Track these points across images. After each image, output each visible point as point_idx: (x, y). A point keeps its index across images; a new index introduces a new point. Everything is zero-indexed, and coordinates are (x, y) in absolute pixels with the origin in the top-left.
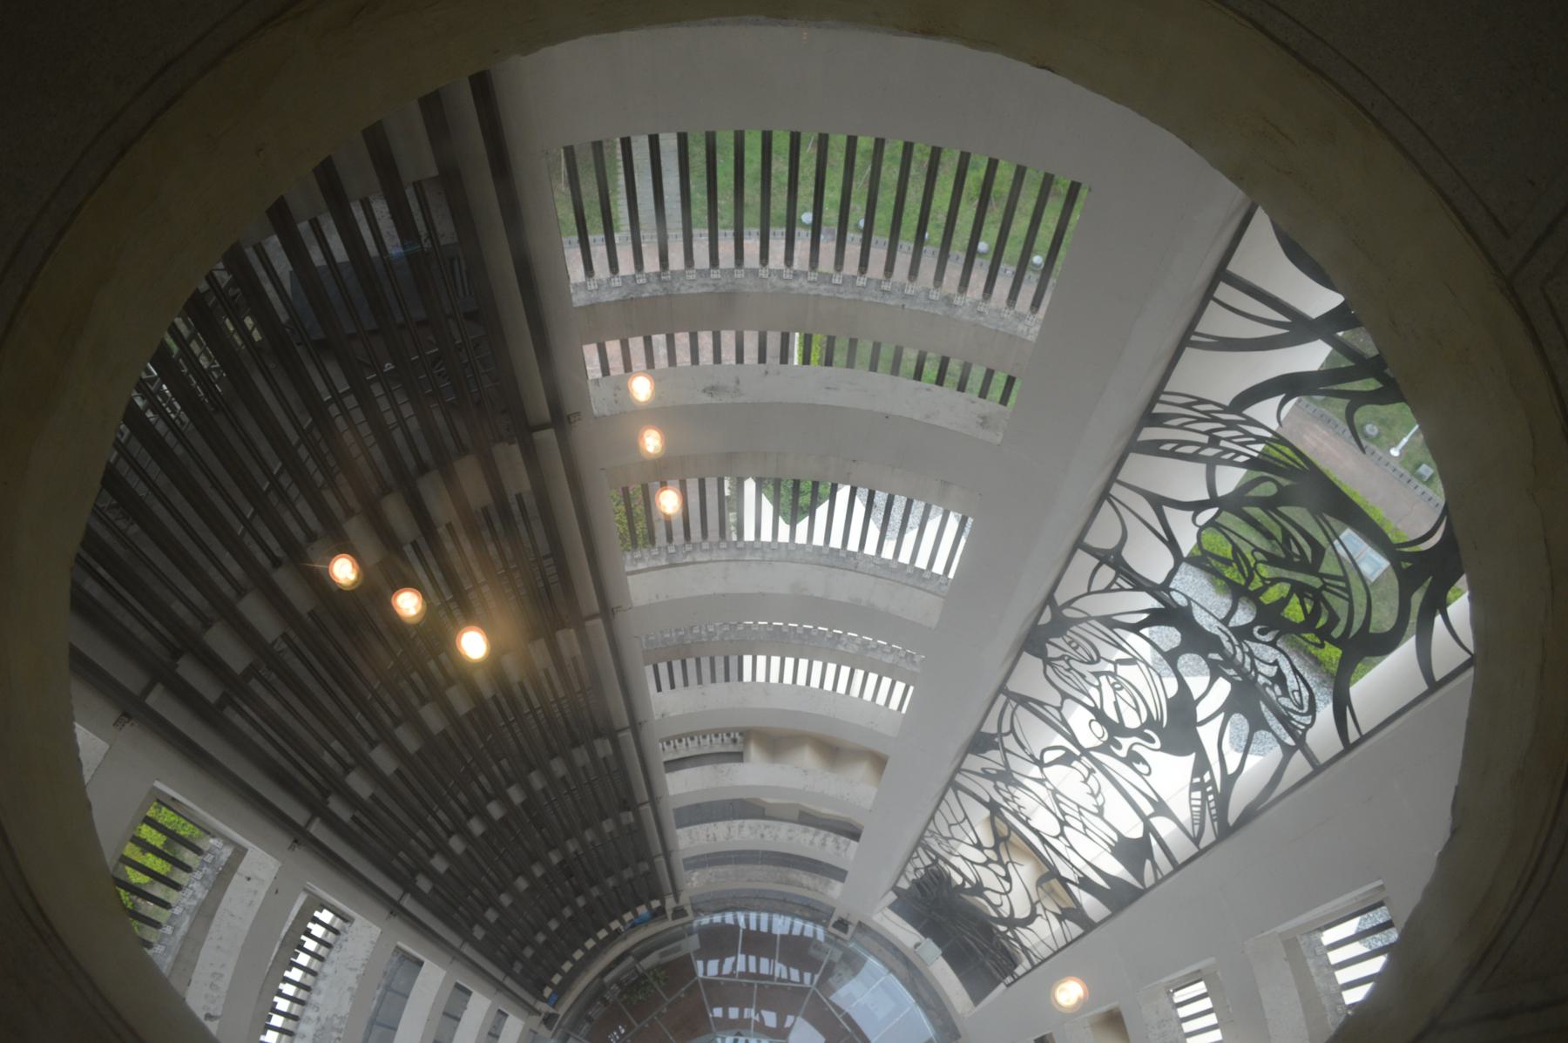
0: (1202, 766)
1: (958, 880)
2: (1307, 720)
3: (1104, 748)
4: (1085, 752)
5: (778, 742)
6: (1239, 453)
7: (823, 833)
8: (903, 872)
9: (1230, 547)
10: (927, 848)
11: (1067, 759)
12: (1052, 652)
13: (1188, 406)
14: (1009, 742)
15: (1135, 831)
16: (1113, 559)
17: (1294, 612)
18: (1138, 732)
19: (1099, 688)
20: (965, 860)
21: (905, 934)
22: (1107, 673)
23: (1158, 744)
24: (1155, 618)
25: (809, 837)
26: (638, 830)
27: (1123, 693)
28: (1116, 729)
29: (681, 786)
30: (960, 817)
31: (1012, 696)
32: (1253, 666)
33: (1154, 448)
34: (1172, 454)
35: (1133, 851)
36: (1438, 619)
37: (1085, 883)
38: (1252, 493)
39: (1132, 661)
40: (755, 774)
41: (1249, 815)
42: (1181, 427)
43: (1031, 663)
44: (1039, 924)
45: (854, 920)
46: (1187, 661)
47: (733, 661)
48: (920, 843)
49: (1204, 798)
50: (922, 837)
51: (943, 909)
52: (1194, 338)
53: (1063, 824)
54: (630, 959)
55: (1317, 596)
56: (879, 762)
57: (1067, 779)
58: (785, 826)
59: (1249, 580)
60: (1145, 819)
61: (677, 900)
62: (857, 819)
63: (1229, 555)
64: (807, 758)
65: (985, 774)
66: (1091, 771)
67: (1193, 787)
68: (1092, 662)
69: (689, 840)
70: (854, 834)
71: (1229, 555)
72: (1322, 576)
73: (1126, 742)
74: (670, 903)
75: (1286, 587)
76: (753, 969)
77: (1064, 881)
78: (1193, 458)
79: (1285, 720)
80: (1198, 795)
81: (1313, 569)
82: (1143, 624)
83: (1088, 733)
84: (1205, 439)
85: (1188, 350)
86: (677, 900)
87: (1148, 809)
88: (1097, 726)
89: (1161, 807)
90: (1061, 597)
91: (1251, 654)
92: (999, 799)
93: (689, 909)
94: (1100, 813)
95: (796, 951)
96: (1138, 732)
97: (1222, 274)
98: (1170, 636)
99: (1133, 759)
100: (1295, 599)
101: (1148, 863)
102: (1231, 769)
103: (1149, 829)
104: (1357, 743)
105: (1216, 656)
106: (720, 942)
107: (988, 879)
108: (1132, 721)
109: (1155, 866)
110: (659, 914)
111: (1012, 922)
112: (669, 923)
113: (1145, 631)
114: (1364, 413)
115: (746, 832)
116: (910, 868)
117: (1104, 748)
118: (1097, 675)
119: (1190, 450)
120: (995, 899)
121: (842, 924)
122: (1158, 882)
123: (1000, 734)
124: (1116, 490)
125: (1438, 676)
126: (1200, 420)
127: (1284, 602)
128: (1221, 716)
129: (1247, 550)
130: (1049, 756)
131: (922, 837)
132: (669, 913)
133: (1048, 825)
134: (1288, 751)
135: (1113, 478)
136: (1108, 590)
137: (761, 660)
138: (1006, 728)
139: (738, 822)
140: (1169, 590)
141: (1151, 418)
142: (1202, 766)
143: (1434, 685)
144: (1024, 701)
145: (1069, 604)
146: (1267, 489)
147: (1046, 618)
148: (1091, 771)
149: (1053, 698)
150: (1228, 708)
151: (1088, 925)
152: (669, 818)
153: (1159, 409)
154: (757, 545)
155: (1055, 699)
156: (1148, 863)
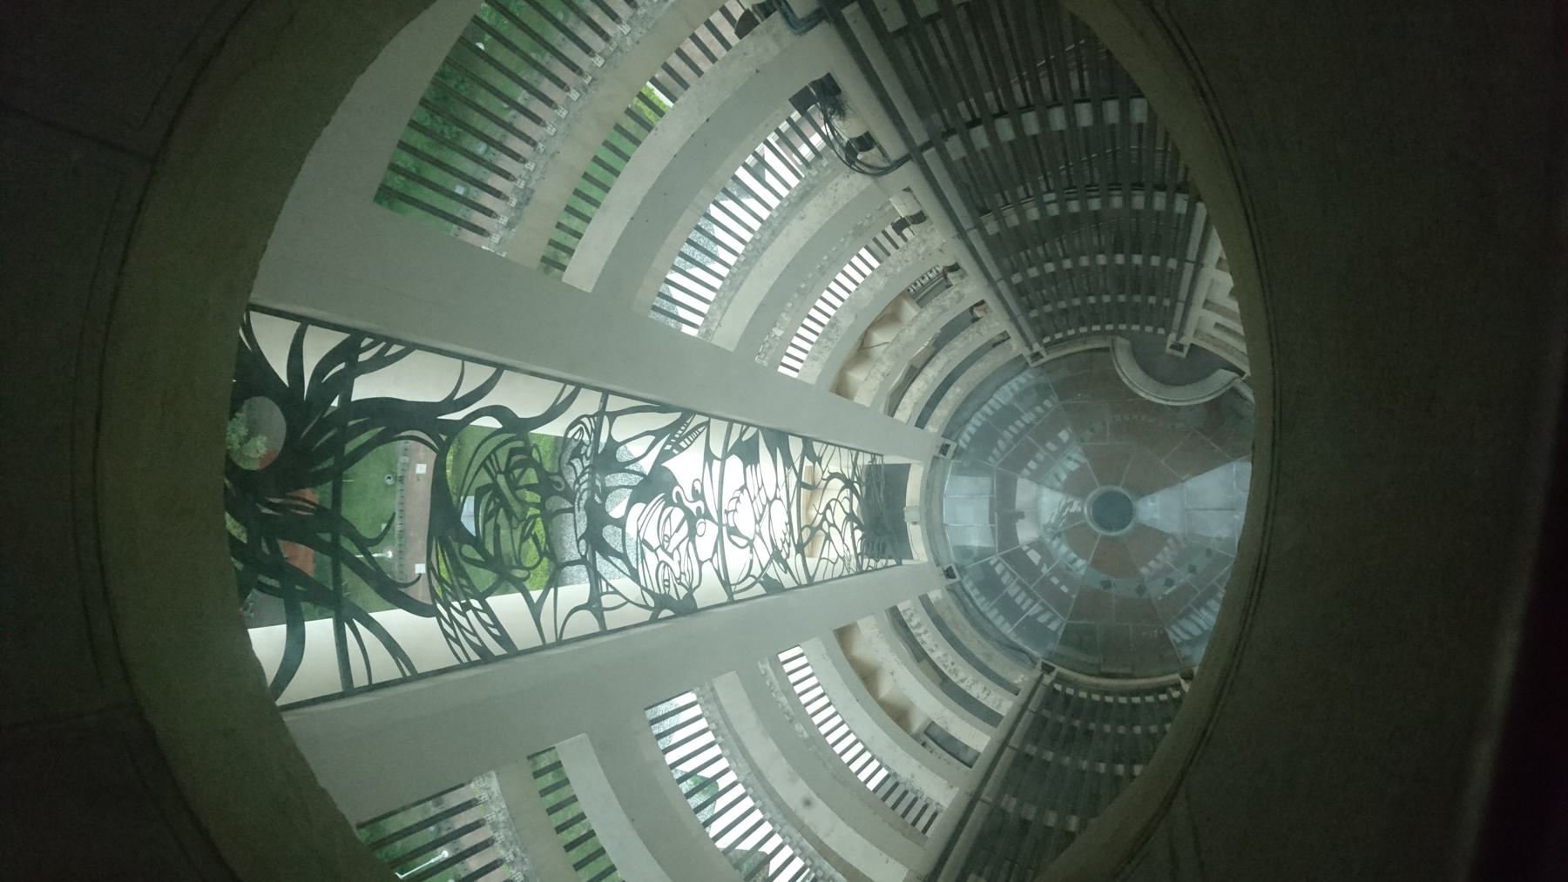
0: (664, 455)
1: (858, 534)
2: (585, 420)
3: (708, 516)
4: (720, 525)
5: (899, 715)
6: (462, 586)
7: (914, 631)
8: (886, 567)
9: (525, 545)
10: (859, 566)
11: (734, 531)
12: (683, 592)
13: (457, 641)
14: (756, 571)
15: (734, 462)
16: (594, 605)
17: (531, 476)
18: (680, 505)
19: (677, 548)
20: (843, 544)
21: (915, 533)
22: (665, 551)
23: (677, 489)
24: (607, 551)
25: (924, 637)
26: (1006, 784)
27: (667, 532)
28: (691, 519)
29: (978, 739)
30: (823, 562)
31: (730, 594)
32: (583, 474)
33: (503, 639)
34: (497, 624)
35: (749, 455)
36: (457, 396)
37: (788, 462)
38: (479, 557)
39: (644, 542)
40: (928, 705)
41: (663, 408)
42: (475, 634)
43: (701, 598)
44: (834, 468)
45: (939, 570)
46: (616, 512)
47: (881, 793)
48: (860, 572)
49: (681, 439)
50: (856, 574)
51: (882, 528)
52: (408, 674)
53: (770, 502)
54: (1103, 670)
55: (508, 472)
56: (844, 635)
57: (744, 520)
58: (934, 656)
59: (534, 517)
60: (723, 461)
61: (1041, 677)
62: (886, 619)
63: (530, 541)
64: (886, 689)
65: (787, 568)
66: (727, 512)
67: (682, 450)
68: (666, 564)
69: (1004, 705)
70: (895, 613)
71: (530, 541)
72: (494, 479)
73: (693, 507)
74: (1047, 679)
75: (518, 493)
76: (1023, 594)
77: (799, 475)
78: (487, 609)
79: (597, 432)
80: (683, 444)
81: (494, 486)
82: (618, 555)
83: (708, 531)
84: (470, 613)
85: (420, 671)
86: (1041, 677)
87: (716, 464)
88: (700, 530)
89: (709, 457)
90: (646, 615)
91: (577, 481)
92: (793, 548)
93: (1039, 666)
94: (744, 488)
95: (990, 584)
96: (680, 505)
97: (349, 690)
98: (610, 534)
99: (698, 495)
100: (522, 483)
101: (744, 438)
102: (651, 438)
103: (726, 455)
104: (571, 383)
105: (597, 499)
106: (1033, 629)
107: (840, 517)
108: (678, 514)
109: (742, 434)
110: (1060, 679)
111: (848, 484)
112: (1058, 669)
113: (620, 549)
114: (368, 533)
115: (962, 675)
116: (879, 565)
117: (708, 516)
118: (671, 555)
119: (484, 616)
120: (846, 504)
121: (949, 574)
122: (749, 425)
123: (757, 580)
124: (550, 638)
125: (491, 371)
126: (460, 626)
127: (530, 487)
128: (631, 467)
129: (517, 534)
130: (742, 542)
131: (856, 574)
132: (1054, 674)
133: (779, 509)
134: (613, 416)
135: (545, 647)
136: (616, 592)
137: (862, 777)
138: (750, 580)
139: (962, 685)
140: (584, 557)
141: (486, 656)
142: (664, 455)
143: (500, 368)
144: (726, 584)
145: (646, 607)
146: (468, 551)
147: (666, 613)
148: (727, 512)
149: (708, 569)
150: (622, 468)
151: (807, 442)
152: (1003, 728)
153: (475, 657)
154: (798, 851)
155: (707, 567)
156: (744, 438)
